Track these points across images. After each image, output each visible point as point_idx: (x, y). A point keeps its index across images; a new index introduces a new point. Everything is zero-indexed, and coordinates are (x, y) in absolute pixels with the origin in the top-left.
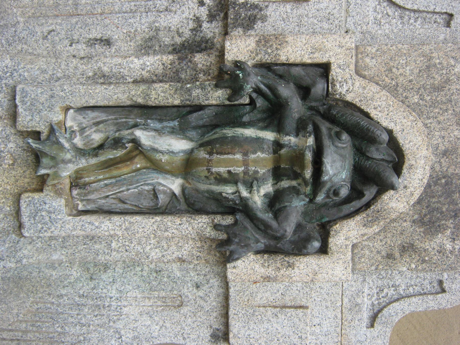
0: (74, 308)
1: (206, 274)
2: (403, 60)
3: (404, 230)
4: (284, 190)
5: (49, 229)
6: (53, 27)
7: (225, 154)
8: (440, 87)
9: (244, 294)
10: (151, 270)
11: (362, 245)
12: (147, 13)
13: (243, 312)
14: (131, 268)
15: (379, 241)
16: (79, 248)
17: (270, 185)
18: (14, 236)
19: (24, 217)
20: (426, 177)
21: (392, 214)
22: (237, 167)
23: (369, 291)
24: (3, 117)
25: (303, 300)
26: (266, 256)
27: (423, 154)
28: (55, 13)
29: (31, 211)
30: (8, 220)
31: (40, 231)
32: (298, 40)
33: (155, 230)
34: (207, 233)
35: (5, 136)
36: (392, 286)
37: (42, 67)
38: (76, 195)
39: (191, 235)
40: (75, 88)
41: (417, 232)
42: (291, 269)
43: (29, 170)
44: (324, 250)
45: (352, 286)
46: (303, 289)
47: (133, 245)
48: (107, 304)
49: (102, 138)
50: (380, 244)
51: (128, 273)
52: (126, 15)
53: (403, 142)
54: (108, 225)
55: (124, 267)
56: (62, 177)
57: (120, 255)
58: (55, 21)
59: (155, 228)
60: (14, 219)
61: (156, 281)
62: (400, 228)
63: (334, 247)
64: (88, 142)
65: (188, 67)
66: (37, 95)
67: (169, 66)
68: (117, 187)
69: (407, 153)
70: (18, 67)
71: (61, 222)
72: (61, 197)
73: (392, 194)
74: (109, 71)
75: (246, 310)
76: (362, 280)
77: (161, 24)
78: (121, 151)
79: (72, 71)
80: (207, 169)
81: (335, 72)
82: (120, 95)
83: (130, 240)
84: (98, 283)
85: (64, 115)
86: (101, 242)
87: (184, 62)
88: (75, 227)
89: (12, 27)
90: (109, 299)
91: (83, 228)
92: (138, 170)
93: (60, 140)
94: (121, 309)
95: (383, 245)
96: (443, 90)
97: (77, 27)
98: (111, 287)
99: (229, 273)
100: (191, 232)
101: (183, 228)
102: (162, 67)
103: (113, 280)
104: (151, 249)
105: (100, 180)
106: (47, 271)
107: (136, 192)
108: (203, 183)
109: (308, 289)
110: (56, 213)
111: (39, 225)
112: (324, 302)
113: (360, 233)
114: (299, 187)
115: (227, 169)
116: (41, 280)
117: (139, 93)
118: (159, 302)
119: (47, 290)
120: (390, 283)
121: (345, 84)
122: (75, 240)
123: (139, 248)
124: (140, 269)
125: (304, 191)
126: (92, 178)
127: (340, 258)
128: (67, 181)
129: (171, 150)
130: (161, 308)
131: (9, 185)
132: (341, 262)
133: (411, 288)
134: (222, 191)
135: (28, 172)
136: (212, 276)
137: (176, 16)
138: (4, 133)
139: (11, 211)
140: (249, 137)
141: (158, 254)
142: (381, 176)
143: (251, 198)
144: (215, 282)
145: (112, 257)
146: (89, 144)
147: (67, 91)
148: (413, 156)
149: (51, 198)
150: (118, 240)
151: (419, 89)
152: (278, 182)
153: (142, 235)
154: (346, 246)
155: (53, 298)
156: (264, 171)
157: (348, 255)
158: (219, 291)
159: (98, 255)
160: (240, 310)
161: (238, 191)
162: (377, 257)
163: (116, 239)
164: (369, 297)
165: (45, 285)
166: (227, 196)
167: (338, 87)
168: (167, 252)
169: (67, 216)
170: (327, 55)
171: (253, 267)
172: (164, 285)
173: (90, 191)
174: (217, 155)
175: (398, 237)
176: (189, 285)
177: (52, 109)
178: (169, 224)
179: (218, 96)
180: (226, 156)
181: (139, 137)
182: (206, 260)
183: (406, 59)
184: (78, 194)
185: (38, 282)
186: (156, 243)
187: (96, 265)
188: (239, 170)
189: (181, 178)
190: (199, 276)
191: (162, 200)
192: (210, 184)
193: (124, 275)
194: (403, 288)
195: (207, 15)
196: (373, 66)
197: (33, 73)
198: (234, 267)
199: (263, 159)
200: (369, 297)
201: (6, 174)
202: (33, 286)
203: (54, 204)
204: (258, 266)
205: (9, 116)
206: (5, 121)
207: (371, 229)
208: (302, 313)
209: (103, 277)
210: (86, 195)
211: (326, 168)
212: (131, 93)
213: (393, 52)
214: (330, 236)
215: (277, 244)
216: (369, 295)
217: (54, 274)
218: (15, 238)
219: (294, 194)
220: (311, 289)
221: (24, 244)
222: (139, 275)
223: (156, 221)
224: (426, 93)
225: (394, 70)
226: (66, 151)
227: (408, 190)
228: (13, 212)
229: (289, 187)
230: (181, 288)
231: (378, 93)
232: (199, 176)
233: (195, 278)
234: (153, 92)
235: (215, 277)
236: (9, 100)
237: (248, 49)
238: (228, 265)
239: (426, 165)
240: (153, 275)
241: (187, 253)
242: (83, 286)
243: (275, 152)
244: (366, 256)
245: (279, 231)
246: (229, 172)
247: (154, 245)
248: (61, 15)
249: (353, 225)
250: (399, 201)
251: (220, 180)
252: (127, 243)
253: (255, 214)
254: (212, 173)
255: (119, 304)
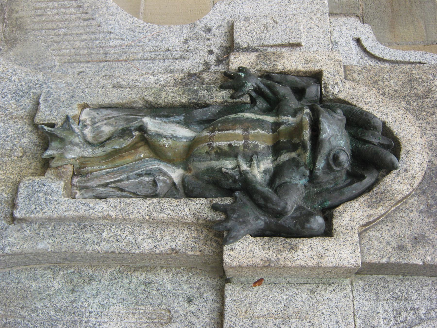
0: (48, 323)
1: (200, 287)
2: (387, 76)
3: (412, 221)
4: (284, 163)
5: (42, 210)
6: (84, 69)
7: (227, 130)
8: (424, 96)
9: (241, 304)
10: (140, 282)
11: (369, 235)
12: (164, 60)
13: (240, 324)
14: (119, 280)
15: (387, 232)
16: (68, 238)
17: (269, 161)
18: (3, 222)
19: (20, 198)
20: (425, 162)
21: (396, 196)
22: (238, 140)
23: (384, 314)
24: (24, 118)
25: (309, 313)
26: (266, 238)
27: (418, 141)
28: (88, 59)
29: (28, 192)
30: (3, 206)
31: (32, 212)
32: (293, 55)
33: (150, 211)
34: (205, 215)
35: (22, 132)
36: (411, 309)
37: (69, 81)
38: (76, 182)
39: (187, 216)
40: (95, 91)
41: (426, 222)
42: (293, 251)
43: (35, 163)
44: (328, 232)
45: (364, 305)
46: (308, 300)
47: (125, 235)
48: (85, 320)
49: (111, 131)
50: (389, 234)
51: (114, 285)
52: (147, 61)
53: (397, 131)
54: (103, 206)
55: (111, 279)
56: (66, 158)
57: (109, 245)
58: (86, 65)
59: (151, 209)
60: (8, 206)
61: (143, 294)
62: (407, 218)
63: (339, 229)
64: (98, 135)
65: (197, 81)
66: (59, 96)
67: (180, 81)
68: (118, 175)
69: (402, 140)
70: (47, 81)
71: (55, 203)
72: (62, 180)
73: (394, 176)
74: (126, 84)
75: (243, 322)
76: (374, 298)
77: (175, 67)
78: (127, 139)
79: (94, 84)
80: (208, 145)
81: (326, 77)
82: (133, 95)
83: (123, 229)
84: (79, 295)
85: (80, 111)
86: (92, 231)
87: (193, 78)
88: (69, 208)
89: (49, 69)
90: (88, 314)
91: (77, 209)
92: (141, 159)
93: (72, 126)
94: (100, 325)
95: (392, 236)
96: (427, 98)
97: (104, 70)
98: (94, 300)
99: (225, 256)
100: (188, 213)
101: (180, 209)
102: (173, 82)
103: (97, 293)
104: (143, 239)
105: (103, 169)
106: (27, 282)
107: (136, 182)
108: (204, 161)
109: (314, 301)
110: (52, 195)
111: (33, 206)
112: (334, 316)
113: (365, 214)
114: (299, 158)
115: (228, 143)
116: (18, 292)
117: (151, 93)
118: (144, 318)
119: (22, 302)
120: (407, 306)
121: (336, 86)
122: (65, 229)
123: (131, 238)
124: (128, 282)
125: (304, 161)
126: (95, 168)
127: (347, 239)
128: (70, 169)
129: (175, 135)
130: (146, 325)
131: (13, 174)
132: (348, 244)
133: (432, 311)
134: (222, 166)
135: (34, 164)
136: (206, 289)
137: (188, 62)
138: (21, 130)
139: (8, 197)
140: (250, 118)
141: (150, 245)
142: (380, 154)
143: (251, 172)
144: (210, 296)
145: (101, 246)
146: (98, 136)
147: (87, 92)
148: (409, 142)
149: (51, 181)
150: (110, 229)
151: (405, 97)
152: (277, 158)
153: (137, 216)
154: (352, 227)
155: (25, 312)
156: (264, 146)
157: (355, 237)
158: (213, 306)
159: (86, 244)
160: (236, 322)
161: (238, 166)
162: (387, 248)
163: (108, 228)
164: (385, 322)
165: (21, 297)
166: (227, 171)
167: (330, 88)
168: (160, 242)
169: (63, 198)
170: (319, 65)
171: (253, 249)
172: (152, 298)
173: (91, 178)
174: (219, 131)
175: (407, 228)
176: (180, 299)
177: (70, 106)
178: (166, 205)
179: (222, 96)
180: (227, 132)
181: (147, 123)
182: (200, 251)
183: (389, 75)
184: (78, 182)
185: (14, 293)
186: (150, 233)
187: (81, 276)
188: (239, 144)
189: (183, 168)
190: (192, 289)
191: (160, 187)
192: (211, 160)
193: (109, 288)
194: (424, 312)
195: (215, 60)
196: (361, 80)
197: (59, 86)
198: (232, 249)
199: (262, 135)
200: (385, 322)
201: (13, 164)
202: (7, 299)
203: (53, 186)
204: (257, 248)
205: (30, 117)
206: (25, 121)
207: (377, 210)
208: (308, 324)
209: (86, 289)
210: (86, 182)
211: (323, 126)
212: (144, 94)
213: (377, 70)
214: (334, 217)
215: (278, 221)
216: (385, 319)
217: (34, 286)
218: (4, 225)
219: (294, 167)
220: (318, 301)
221: (11, 231)
222: (126, 288)
223: (153, 203)
224: (412, 100)
225: (380, 83)
226: (76, 135)
227: (409, 173)
228: (10, 199)
229: (289, 160)
230: (171, 302)
231: (367, 92)
232: (200, 153)
233: (188, 292)
234: (164, 93)
235: (210, 291)
236: (33, 105)
237: (249, 61)
238: (225, 248)
239: (422, 152)
240: (142, 287)
241: (182, 244)
242: (62, 298)
243: (274, 131)
244: (375, 247)
245: (280, 203)
246: (230, 145)
247: (147, 235)
248: (92, 61)
249: (357, 206)
250: (401, 183)
251: (221, 154)
252: (119, 233)
253: (255, 186)
254: (213, 147)
255: (99, 320)
